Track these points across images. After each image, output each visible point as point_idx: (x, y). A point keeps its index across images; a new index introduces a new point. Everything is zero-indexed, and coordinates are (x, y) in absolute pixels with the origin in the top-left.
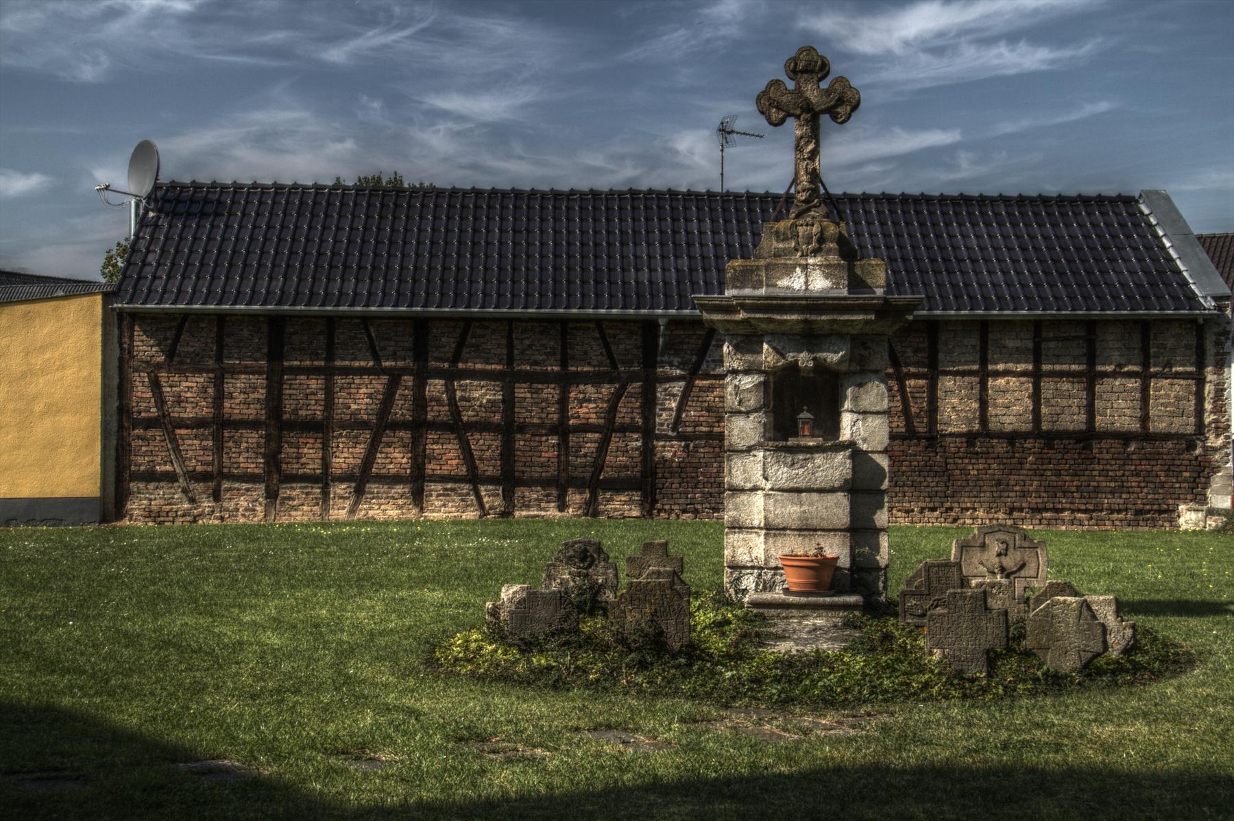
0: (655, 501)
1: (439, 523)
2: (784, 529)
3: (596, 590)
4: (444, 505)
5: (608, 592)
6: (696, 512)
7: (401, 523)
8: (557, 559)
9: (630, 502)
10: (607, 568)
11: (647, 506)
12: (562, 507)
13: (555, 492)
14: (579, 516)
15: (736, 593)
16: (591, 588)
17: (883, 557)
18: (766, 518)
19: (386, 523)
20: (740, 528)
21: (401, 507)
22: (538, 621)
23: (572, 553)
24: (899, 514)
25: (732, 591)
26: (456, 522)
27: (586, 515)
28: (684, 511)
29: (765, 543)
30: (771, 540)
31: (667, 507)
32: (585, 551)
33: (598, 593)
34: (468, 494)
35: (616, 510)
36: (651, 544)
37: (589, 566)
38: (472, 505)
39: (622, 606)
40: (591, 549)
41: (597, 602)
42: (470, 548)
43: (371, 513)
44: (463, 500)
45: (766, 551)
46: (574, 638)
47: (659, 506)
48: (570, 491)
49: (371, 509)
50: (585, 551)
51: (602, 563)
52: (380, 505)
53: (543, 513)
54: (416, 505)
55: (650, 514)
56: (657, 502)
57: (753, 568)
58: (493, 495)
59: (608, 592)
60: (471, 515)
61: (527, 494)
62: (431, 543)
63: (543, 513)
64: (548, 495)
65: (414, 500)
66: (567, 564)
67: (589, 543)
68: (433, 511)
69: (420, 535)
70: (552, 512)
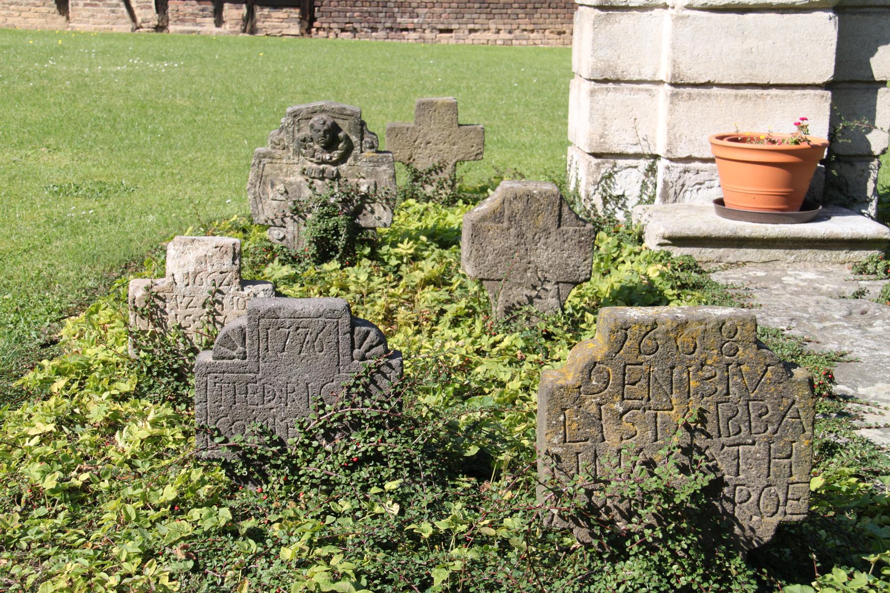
0: (313, 19)
1: (86, 35)
2: (708, 85)
3: (355, 205)
4: (93, 16)
5: (379, 209)
6: (354, 31)
7: (43, 34)
8: (275, 145)
9: (288, 19)
10: (377, 163)
11: (306, 24)
12: (219, 22)
13: (210, 7)
14: (237, 33)
15: (605, 201)
16: (346, 202)
17: (877, 141)
18: (675, 64)
19: (24, 34)
20: (617, 81)
21: (44, 16)
22: (286, 393)
23: (306, 132)
24: (552, 35)
25: (598, 200)
26: (106, 36)
27: (244, 31)
28: (343, 30)
29: (671, 112)
30: (600, 97)
31: (325, 25)
32: (334, 129)
33: (358, 211)
34: (118, 5)
35: (274, 27)
36: (431, 104)
37: (343, 159)
38: (123, 17)
39: (590, 404)
40: (345, 126)
41: (361, 229)
42: (117, 73)
43: (10, 21)
44: (113, 12)
45: (671, 127)
46: (391, 444)
47: (317, 24)
48: (226, 6)
49: (10, 15)
50: (334, 129)
51: (368, 153)
52: (21, 11)
53: (198, 28)
54: (62, 14)
55: (308, 31)
56: (315, 20)
57: (637, 156)
58: (145, 7)
59: (379, 209)
60: (124, 26)
61: (181, 7)
62: (70, 64)
63: (198, 28)
64: (203, 10)
65: (59, 8)
66: (298, 153)
67: (342, 113)
68: (80, 22)
69: (59, 50)
70: (208, 25)
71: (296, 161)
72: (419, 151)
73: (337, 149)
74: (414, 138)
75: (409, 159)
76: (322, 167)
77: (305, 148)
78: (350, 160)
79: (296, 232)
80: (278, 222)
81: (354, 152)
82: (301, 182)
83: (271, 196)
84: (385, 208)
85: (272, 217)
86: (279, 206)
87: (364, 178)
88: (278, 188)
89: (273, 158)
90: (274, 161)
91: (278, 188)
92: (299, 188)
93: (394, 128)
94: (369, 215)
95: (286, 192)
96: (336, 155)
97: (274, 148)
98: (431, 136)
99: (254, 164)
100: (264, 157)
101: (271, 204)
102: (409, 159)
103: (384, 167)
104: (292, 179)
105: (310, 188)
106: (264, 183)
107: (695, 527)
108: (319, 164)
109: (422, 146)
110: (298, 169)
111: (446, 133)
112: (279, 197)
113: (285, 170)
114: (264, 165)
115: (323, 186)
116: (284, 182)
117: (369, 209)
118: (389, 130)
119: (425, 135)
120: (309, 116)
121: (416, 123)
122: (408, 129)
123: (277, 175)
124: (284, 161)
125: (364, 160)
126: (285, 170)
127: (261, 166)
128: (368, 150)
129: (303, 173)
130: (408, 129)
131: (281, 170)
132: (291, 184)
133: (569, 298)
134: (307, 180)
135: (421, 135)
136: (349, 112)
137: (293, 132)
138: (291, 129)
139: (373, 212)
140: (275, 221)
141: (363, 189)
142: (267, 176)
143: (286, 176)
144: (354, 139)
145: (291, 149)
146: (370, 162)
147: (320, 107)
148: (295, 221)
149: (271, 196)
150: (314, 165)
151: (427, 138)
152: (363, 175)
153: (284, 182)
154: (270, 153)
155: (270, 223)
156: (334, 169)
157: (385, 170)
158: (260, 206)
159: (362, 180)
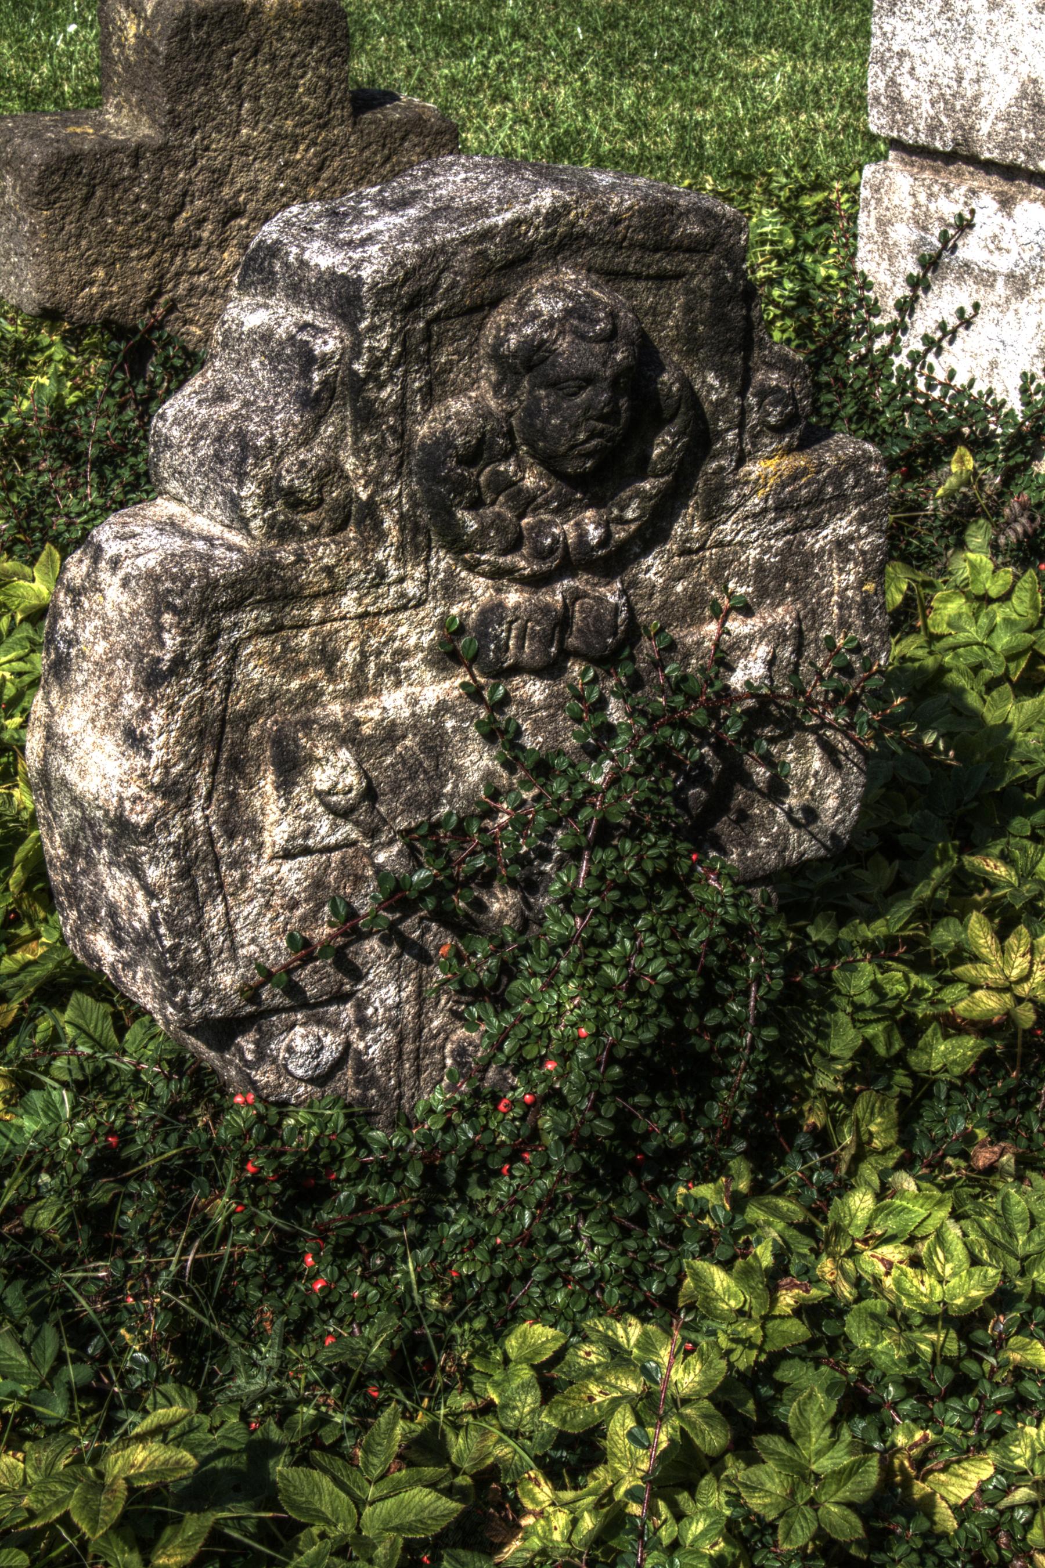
75: (150, 304)
76: (556, 596)
83: (277, 832)
87: (747, 610)
88: (322, 778)
98: (241, 180)
99: (179, 662)
100: (235, 605)
102: (150, 304)
103: (843, 526)
104: (392, 703)
107: (446, 1191)
113: (350, 657)
114: (234, 651)
115: (555, 704)
116: (349, 736)
117: (761, 773)
119: (219, 177)
121: (175, 121)
123: (311, 695)
124: (348, 603)
125: (756, 502)
126: (350, 657)
127: (221, 660)
132: (390, 733)
133: (1012, 841)
135: (201, 182)
143: (358, 692)
146: (781, 508)
149: (277, 832)
151: (226, 192)
153: (349, 736)
157: (840, 544)
158: (215, 912)
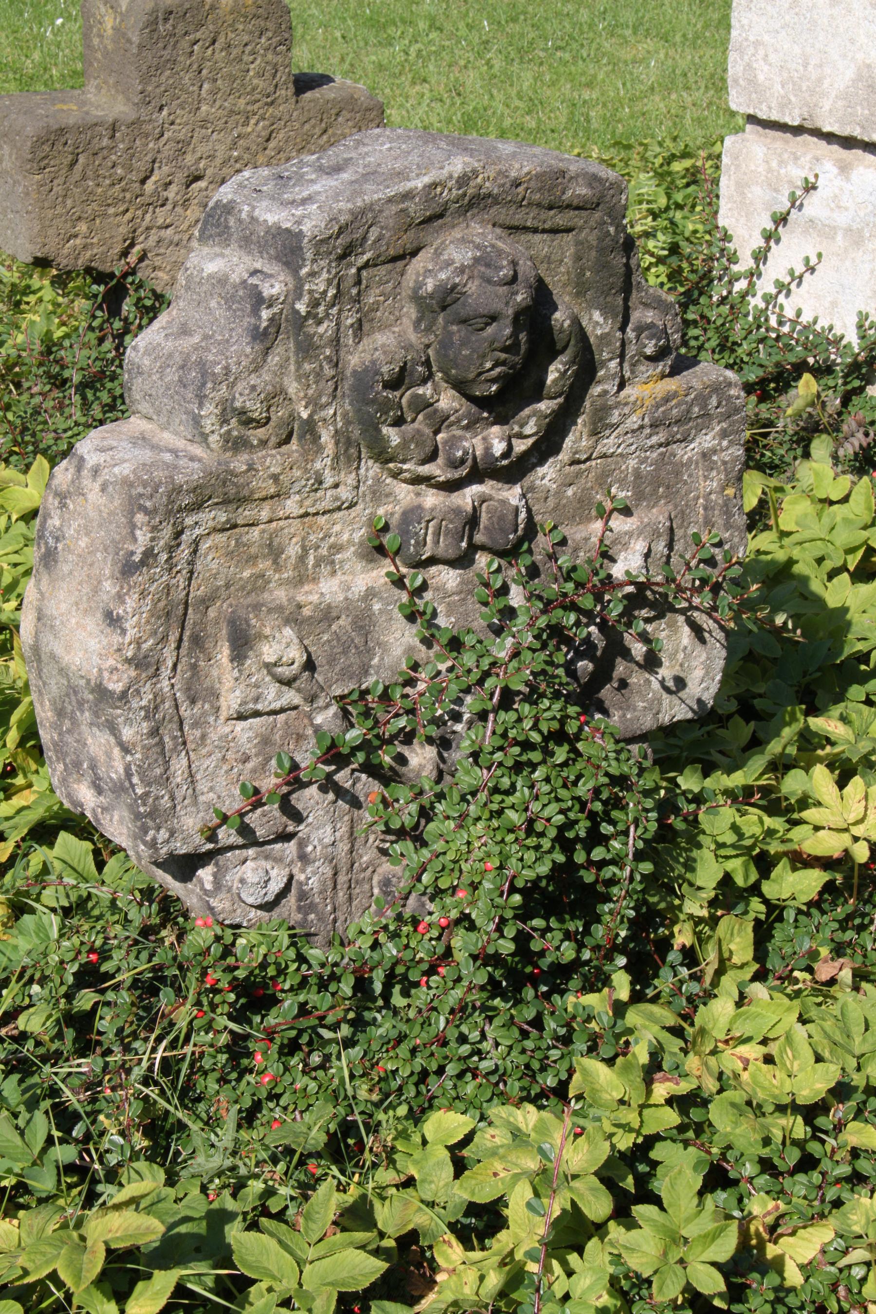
23: (390, 340)
71: (345, 493)
72: (162, 216)
73: (538, 397)
74: (141, 165)
75: (125, 253)
77: (399, 422)
78: (576, 439)
79: (343, 847)
80: (264, 821)
81: (596, 390)
82: (370, 594)
84: (698, 631)
85: (234, 803)
86: (265, 741)
87: (627, 511)
88: (269, 652)
89: (241, 500)
90: (246, 514)
91: (269, 652)
92: (364, 623)
93: (62, 131)
94: (637, 678)
95: (310, 665)
96: (531, 422)
97: (236, 444)
100: (197, 507)
101: (227, 741)
102: (125, 253)
103: (707, 440)
104: (328, 589)
105: (411, 618)
106: (197, 641)
108: (452, 486)
109: (171, 193)
110: (351, 531)
111: (255, 128)
112: (273, 696)
113: (293, 550)
114: (196, 543)
115: (465, 590)
116: (293, 617)
118: (41, 141)
119: (182, 147)
120: (408, 240)
122: (114, 128)
123: (260, 583)
124: (291, 505)
125: (634, 421)
126: (293, 550)
128: (647, 370)
129: (380, 550)
130: (114, 128)
131: (275, 552)
132: (327, 615)
134: (399, 582)
135: (168, 151)
136: (583, 190)
137: (336, 342)
138: (325, 329)
139: (652, 662)
140: (253, 819)
141: (627, 564)
142: (206, 602)
143: (300, 580)
144: (598, 323)
145: (326, 437)
147: (464, 180)
148: (340, 792)
150: (431, 499)
151: (189, 159)
152: (623, 494)
154: (226, 477)
155: (227, 835)
156: (513, 495)
158: (179, 765)
159: (618, 523)
